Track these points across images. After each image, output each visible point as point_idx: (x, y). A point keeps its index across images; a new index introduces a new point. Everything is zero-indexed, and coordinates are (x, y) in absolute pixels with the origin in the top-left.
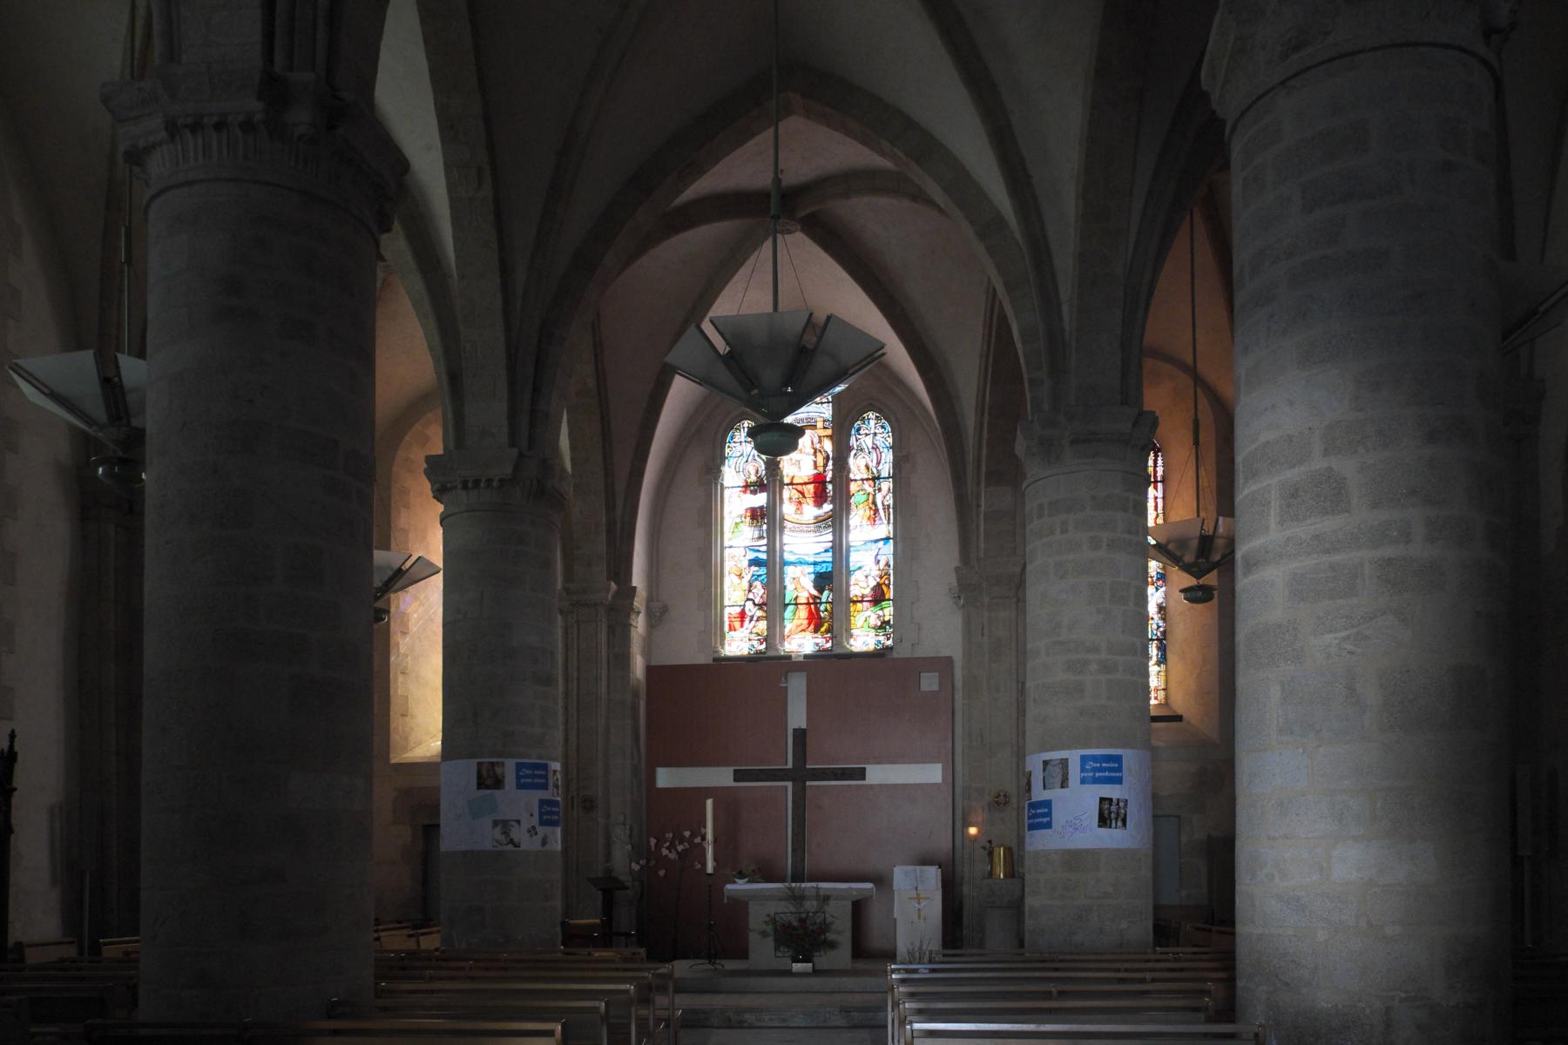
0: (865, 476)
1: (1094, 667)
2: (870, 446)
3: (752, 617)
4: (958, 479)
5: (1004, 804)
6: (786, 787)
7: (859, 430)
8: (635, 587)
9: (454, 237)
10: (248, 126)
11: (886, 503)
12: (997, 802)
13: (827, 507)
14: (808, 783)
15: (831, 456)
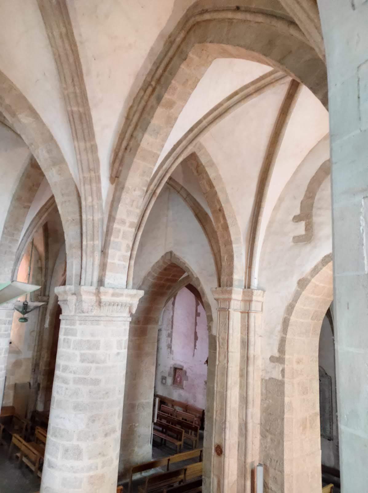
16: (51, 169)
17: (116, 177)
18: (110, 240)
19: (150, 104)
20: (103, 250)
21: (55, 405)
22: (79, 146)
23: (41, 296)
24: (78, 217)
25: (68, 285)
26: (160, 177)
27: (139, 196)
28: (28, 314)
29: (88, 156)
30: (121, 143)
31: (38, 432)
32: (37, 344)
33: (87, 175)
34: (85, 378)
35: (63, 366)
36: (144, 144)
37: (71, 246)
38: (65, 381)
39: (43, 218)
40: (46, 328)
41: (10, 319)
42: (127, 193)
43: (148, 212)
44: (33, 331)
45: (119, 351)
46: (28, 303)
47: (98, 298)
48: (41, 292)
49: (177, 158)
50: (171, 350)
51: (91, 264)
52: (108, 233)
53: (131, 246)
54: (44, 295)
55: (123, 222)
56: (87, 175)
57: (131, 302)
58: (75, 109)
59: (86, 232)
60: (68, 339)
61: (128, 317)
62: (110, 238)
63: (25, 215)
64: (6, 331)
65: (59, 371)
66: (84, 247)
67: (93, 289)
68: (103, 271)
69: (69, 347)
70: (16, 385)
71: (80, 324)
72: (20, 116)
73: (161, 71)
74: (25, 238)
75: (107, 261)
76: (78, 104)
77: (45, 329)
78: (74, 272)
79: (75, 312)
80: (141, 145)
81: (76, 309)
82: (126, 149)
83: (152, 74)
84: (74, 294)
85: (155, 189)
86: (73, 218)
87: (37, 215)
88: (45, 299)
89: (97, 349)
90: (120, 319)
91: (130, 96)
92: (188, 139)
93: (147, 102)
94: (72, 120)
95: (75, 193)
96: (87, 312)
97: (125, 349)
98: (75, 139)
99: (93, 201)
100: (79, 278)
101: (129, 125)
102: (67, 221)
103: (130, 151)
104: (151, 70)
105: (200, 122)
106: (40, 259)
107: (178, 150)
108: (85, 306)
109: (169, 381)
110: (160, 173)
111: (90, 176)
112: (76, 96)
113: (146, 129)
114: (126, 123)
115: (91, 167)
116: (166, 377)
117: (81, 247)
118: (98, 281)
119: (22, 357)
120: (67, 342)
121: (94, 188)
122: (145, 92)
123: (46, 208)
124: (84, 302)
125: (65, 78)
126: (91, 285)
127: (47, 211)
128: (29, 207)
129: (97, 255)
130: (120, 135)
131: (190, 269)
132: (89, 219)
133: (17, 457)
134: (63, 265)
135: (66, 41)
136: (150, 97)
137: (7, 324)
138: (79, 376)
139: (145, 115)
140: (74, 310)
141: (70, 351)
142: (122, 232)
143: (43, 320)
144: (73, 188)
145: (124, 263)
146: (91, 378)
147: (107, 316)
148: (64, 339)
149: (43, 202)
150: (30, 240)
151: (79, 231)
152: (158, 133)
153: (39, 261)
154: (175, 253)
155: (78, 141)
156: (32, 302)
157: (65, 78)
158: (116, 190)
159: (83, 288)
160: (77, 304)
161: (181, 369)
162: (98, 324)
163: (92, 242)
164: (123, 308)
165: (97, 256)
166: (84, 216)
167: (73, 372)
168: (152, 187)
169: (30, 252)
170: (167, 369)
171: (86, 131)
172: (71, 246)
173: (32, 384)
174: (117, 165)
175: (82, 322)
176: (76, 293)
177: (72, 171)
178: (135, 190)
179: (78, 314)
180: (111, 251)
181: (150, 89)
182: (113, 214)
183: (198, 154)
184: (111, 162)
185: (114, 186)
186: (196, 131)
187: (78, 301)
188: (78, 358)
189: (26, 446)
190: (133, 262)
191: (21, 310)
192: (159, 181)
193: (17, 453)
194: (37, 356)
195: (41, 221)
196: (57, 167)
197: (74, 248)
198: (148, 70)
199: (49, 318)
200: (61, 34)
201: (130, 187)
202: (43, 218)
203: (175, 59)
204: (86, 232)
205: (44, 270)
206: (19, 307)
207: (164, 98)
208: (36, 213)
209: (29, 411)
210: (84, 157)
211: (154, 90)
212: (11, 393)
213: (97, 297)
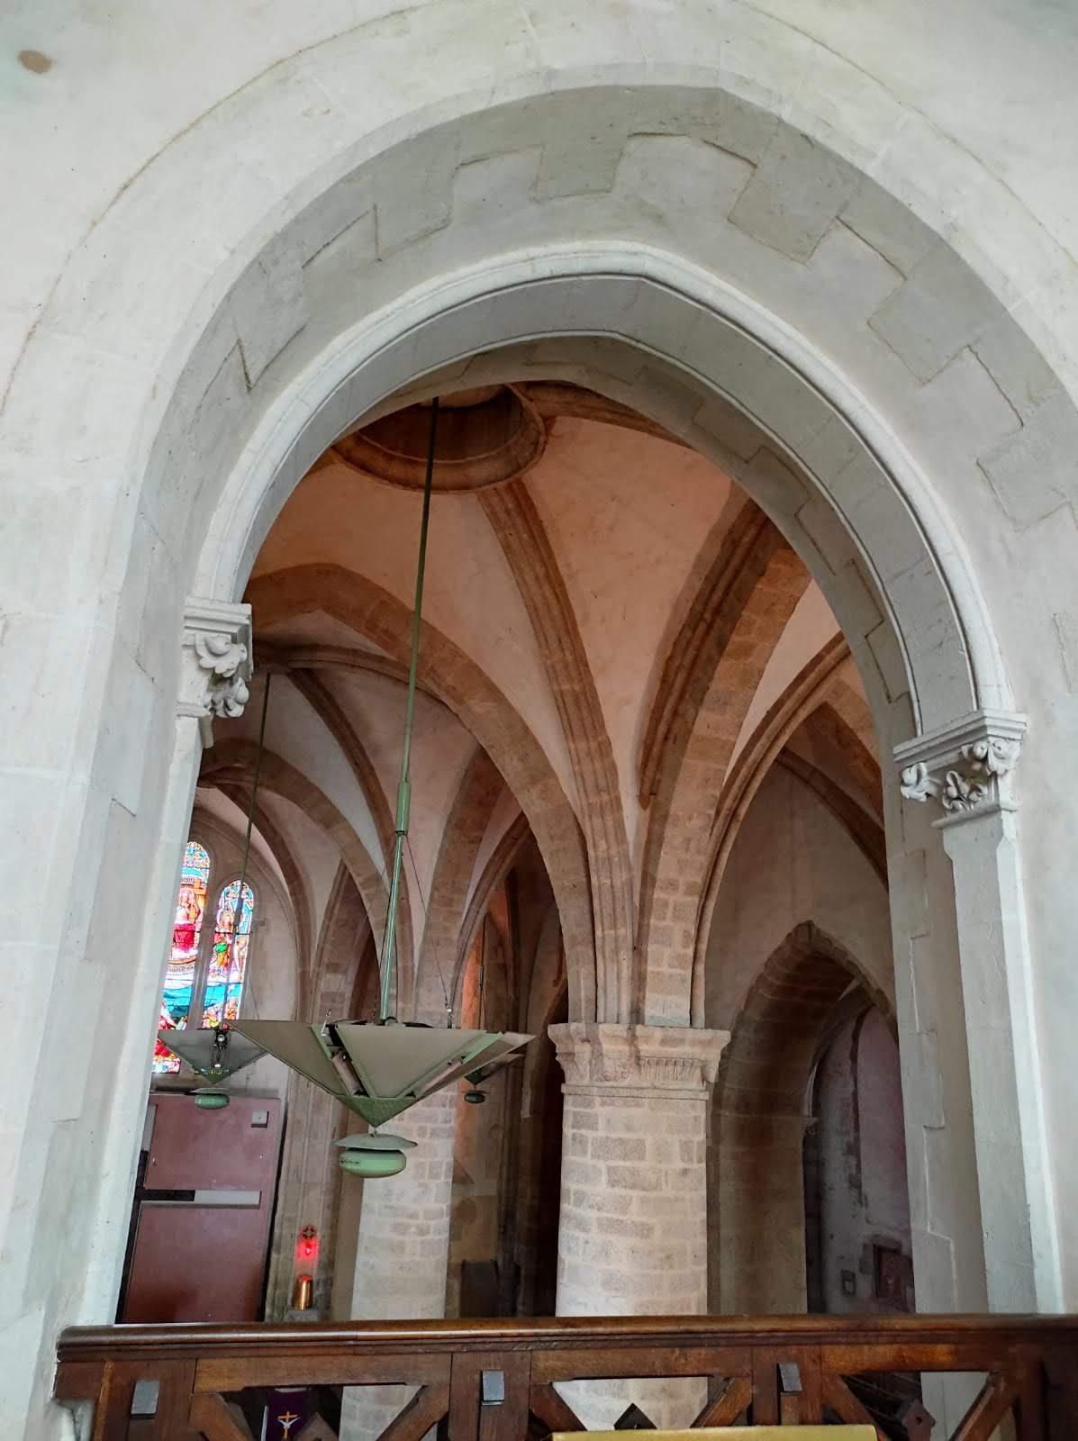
0: (228, 931)
1: (413, 1229)
4: (303, 959)
5: (307, 1229)
7: (228, 893)
11: (241, 954)
13: (193, 952)
15: (202, 911)
17: (651, 794)
18: (648, 925)
19: (704, 656)
20: (635, 945)
22: (576, 749)
26: (744, 782)
27: (700, 828)
29: (593, 764)
30: (657, 727)
32: (506, 1160)
33: (593, 799)
34: (622, 1221)
36: (700, 728)
39: (508, 860)
40: (525, 1119)
42: (676, 826)
43: (725, 856)
44: (496, 1126)
45: (687, 1166)
47: (633, 1048)
49: (777, 738)
50: (860, 1193)
51: (615, 974)
52: (644, 910)
53: (693, 932)
55: (672, 885)
56: (593, 799)
57: (703, 1057)
58: (566, 687)
59: (601, 911)
60: (582, 1136)
61: (701, 1091)
62: (649, 919)
63: (472, 859)
64: (446, 1122)
66: (598, 942)
67: (622, 1030)
68: (639, 990)
69: (585, 1152)
70: (464, 1264)
71: (603, 1104)
72: (472, 702)
73: (720, 594)
75: (646, 969)
76: (570, 679)
79: (591, 1077)
80: (695, 730)
81: (591, 1072)
82: (666, 738)
83: (703, 599)
85: (735, 806)
86: (574, 883)
87: (495, 854)
89: (639, 1159)
90: (682, 1095)
91: (666, 639)
92: (795, 696)
93: (699, 649)
94: (561, 705)
96: (615, 1080)
97: (700, 1161)
98: (570, 736)
99: (609, 848)
101: (669, 694)
102: (563, 888)
103: (674, 742)
104: (701, 593)
105: (818, 659)
106: (501, 943)
107: (778, 719)
108: (609, 1066)
109: (865, 1285)
110: (744, 771)
111: (601, 801)
112: (566, 666)
113: (702, 700)
114: (662, 689)
115: (602, 783)
116: (854, 1275)
118: (632, 1013)
119: (474, 1192)
120: (581, 1141)
121: (610, 823)
122: (694, 632)
124: (205, 1375)
125: (546, 640)
126: (618, 1022)
127: (514, 844)
128: (481, 839)
129: (625, 957)
130: (653, 712)
131: (861, 969)
132: (604, 884)
134: (555, 959)
135: (546, 587)
136: (703, 641)
137: (448, 1106)
138: (609, 1216)
139: (698, 673)
141: (588, 1160)
142: (671, 908)
144: (571, 821)
145: (683, 972)
146: (633, 1222)
147: (655, 1088)
148: (574, 1135)
149: (507, 826)
151: (587, 908)
152: (726, 703)
153: (500, 948)
154: (820, 926)
155: (574, 740)
157: (546, 640)
158: (652, 819)
159: (604, 1029)
160: (594, 1062)
161: (896, 1252)
162: (637, 1105)
163: (612, 932)
164: (688, 1069)
165: (626, 957)
166: (594, 880)
168: (728, 802)
170: (857, 1252)
171: (588, 722)
173: (500, 1263)
174: (650, 773)
175: (606, 1099)
176: (590, 1039)
177: (565, 790)
178: (690, 819)
179: (597, 1084)
180: (651, 948)
181: (702, 627)
182: (650, 870)
183: (835, 706)
184: (640, 763)
185: (648, 812)
186: (812, 677)
188: (604, 1178)
190: (701, 969)
192: (743, 788)
195: (505, 867)
196: (539, 787)
197: (579, 943)
198: (697, 592)
200: (537, 578)
201: (680, 813)
202: (508, 860)
203: (745, 571)
204: (601, 911)
205: (511, 972)
207: (731, 642)
210: (587, 768)
211: (710, 627)
213: (630, 1045)
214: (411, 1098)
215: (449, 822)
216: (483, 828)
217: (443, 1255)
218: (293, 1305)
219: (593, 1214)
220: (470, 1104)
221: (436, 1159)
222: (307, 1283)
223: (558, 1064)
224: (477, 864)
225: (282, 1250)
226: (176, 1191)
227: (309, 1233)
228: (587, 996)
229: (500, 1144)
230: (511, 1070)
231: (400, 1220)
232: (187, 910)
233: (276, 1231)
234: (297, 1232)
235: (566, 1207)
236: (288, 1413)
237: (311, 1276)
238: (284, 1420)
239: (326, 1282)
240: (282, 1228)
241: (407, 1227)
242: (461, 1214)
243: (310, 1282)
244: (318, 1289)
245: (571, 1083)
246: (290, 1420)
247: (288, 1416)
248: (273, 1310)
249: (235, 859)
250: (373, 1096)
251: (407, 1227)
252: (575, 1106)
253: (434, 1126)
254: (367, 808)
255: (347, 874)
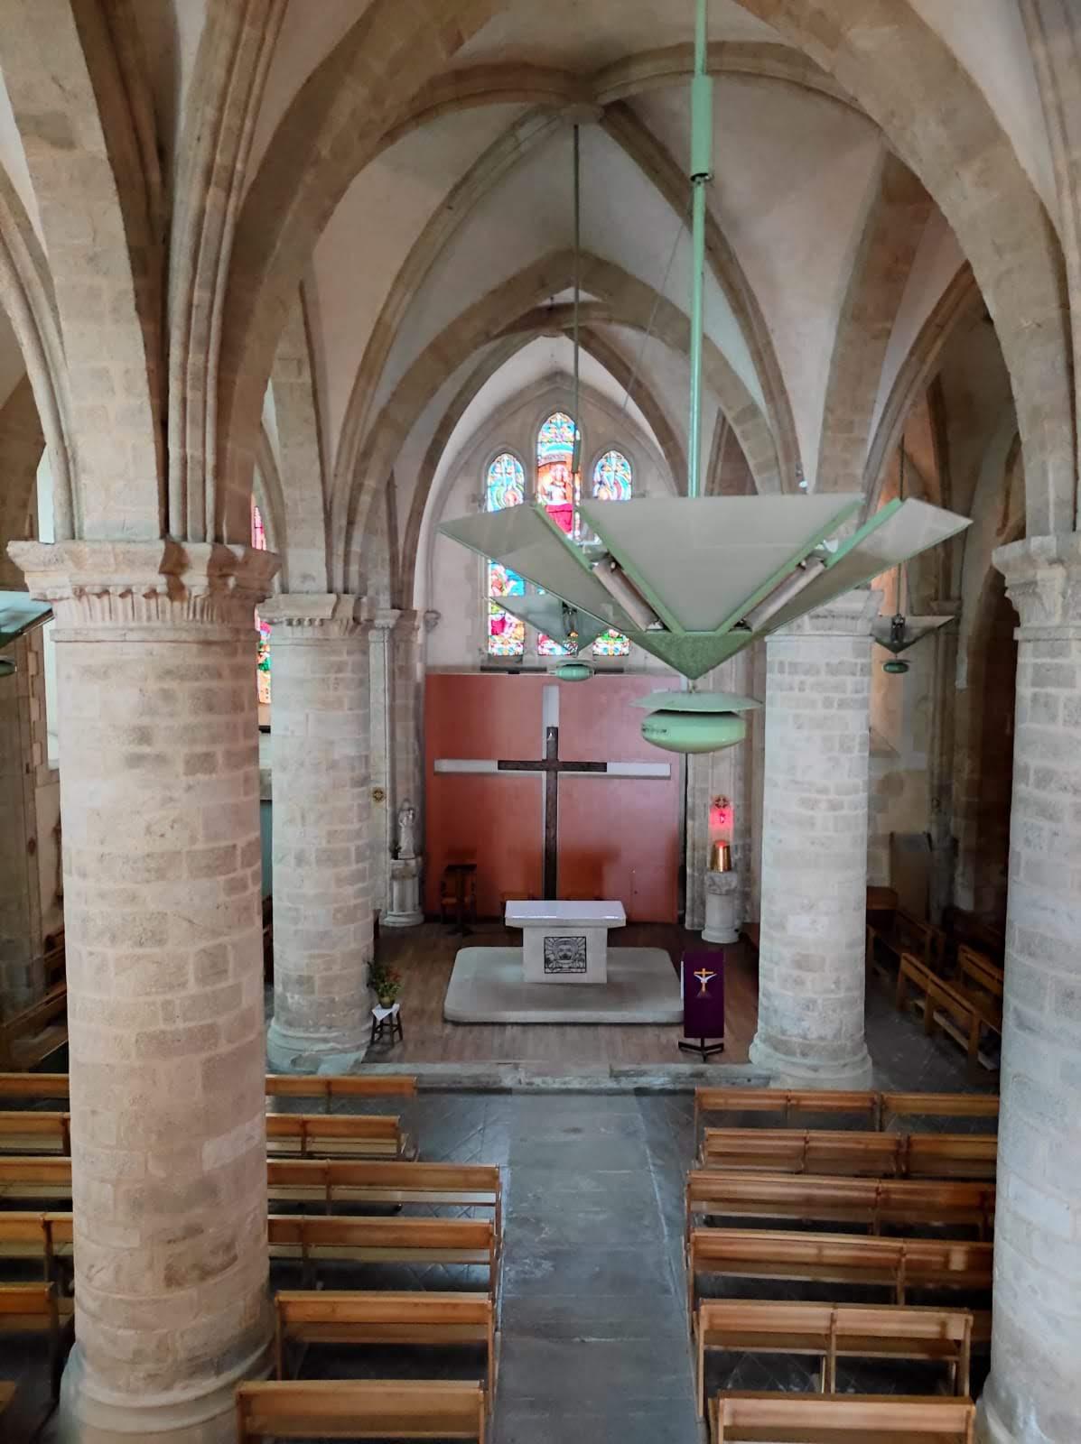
1: (823, 805)
2: (612, 481)
3: (511, 624)
6: (541, 779)
7: (603, 467)
8: (416, 611)
9: (277, 415)
10: (152, 594)
12: (717, 805)
14: (559, 773)
16: (957, 174)
21: (1022, 875)
22: (1050, 57)
23: (936, 599)
24: (1054, 313)
25: (1034, 535)
28: (907, 649)
31: (967, 958)
32: (938, 731)
35: (1036, 772)
37: (1036, 413)
38: (1047, 812)
39: (931, 358)
40: (961, 691)
41: (863, 660)
44: (925, 698)
46: (904, 619)
48: (937, 591)
54: (947, 597)
60: (1047, 695)
63: (877, 363)
64: (857, 692)
65: (1027, 784)
69: (1053, 718)
74: (884, 431)
77: (957, 694)
78: (1052, 496)
84: (1058, 561)
86: (1037, 321)
87: (911, 353)
88: (951, 606)
95: (1041, 232)
100: (1069, 511)
117: (592, 1028)
119: (901, 766)
120: (1047, 704)
123: (938, 326)
128: (889, 333)
133: (919, 1010)
137: (858, 673)
140: (1060, 612)
143: (948, 670)
148: (1035, 698)
150: (894, 442)
156: (915, 615)
160: (1069, 592)
167: (1069, 787)
169: (897, 478)
172: (1036, 413)
176: (1064, 558)
187: (1072, 583)
189: (936, 984)
191: (887, 640)
193: (918, 999)
194: (941, 765)
196: (977, 165)
199: (966, 660)
202: (931, 358)
206: (882, 631)
208: (907, 351)
209: (934, 905)
212: (884, 855)
214: (741, 632)
215: (843, 316)
216: (890, 315)
217: (862, 830)
218: (712, 868)
219: (1067, 799)
220: (892, 675)
221: (847, 733)
222: (724, 848)
223: (1008, 602)
224: (886, 366)
225: (697, 817)
226: (589, 763)
227: (721, 803)
228: (1058, 497)
229: (930, 716)
230: (942, 638)
231: (806, 795)
232: (563, 489)
233: (689, 800)
234: (710, 802)
235: (1020, 789)
236: (704, 970)
237: (728, 842)
238: (701, 975)
239: (744, 847)
240: (694, 796)
241: (816, 802)
242: (884, 791)
243: (727, 848)
244: (737, 853)
245: (1029, 625)
246: (707, 976)
247: (704, 972)
248: (694, 871)
249: (603, 426)
250: (677, 630)
251: (816, 802)
252: (1037, 657)
253: (842, 696)
254: (729, 310)
255: (727, 427)
